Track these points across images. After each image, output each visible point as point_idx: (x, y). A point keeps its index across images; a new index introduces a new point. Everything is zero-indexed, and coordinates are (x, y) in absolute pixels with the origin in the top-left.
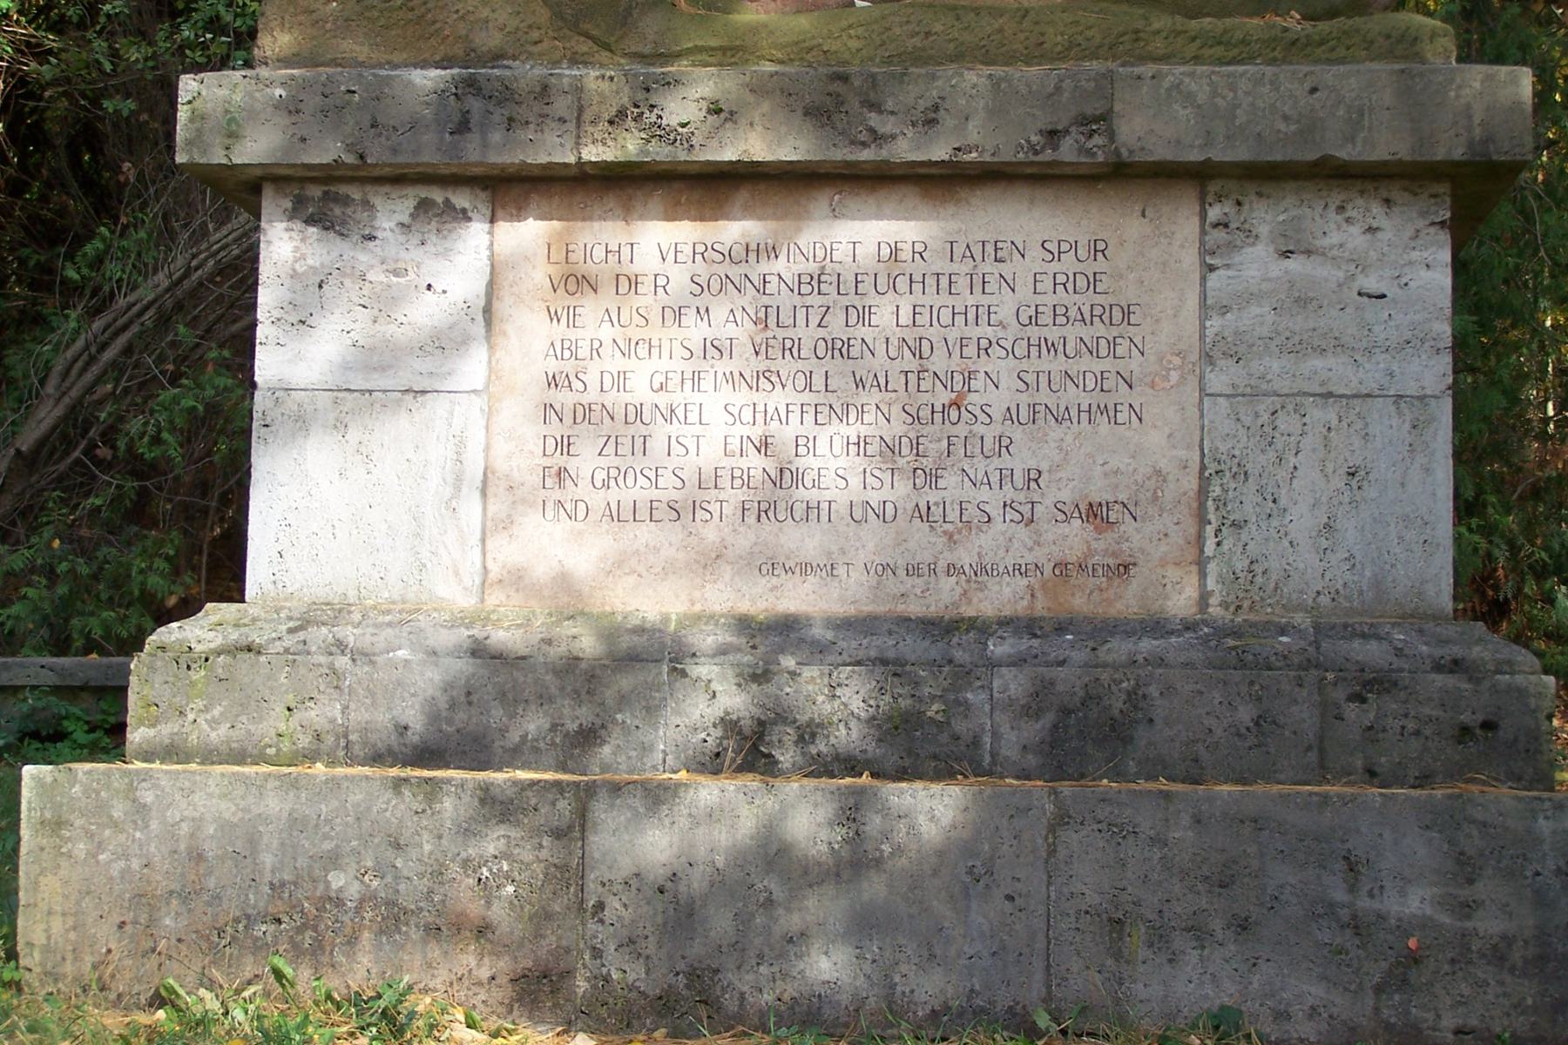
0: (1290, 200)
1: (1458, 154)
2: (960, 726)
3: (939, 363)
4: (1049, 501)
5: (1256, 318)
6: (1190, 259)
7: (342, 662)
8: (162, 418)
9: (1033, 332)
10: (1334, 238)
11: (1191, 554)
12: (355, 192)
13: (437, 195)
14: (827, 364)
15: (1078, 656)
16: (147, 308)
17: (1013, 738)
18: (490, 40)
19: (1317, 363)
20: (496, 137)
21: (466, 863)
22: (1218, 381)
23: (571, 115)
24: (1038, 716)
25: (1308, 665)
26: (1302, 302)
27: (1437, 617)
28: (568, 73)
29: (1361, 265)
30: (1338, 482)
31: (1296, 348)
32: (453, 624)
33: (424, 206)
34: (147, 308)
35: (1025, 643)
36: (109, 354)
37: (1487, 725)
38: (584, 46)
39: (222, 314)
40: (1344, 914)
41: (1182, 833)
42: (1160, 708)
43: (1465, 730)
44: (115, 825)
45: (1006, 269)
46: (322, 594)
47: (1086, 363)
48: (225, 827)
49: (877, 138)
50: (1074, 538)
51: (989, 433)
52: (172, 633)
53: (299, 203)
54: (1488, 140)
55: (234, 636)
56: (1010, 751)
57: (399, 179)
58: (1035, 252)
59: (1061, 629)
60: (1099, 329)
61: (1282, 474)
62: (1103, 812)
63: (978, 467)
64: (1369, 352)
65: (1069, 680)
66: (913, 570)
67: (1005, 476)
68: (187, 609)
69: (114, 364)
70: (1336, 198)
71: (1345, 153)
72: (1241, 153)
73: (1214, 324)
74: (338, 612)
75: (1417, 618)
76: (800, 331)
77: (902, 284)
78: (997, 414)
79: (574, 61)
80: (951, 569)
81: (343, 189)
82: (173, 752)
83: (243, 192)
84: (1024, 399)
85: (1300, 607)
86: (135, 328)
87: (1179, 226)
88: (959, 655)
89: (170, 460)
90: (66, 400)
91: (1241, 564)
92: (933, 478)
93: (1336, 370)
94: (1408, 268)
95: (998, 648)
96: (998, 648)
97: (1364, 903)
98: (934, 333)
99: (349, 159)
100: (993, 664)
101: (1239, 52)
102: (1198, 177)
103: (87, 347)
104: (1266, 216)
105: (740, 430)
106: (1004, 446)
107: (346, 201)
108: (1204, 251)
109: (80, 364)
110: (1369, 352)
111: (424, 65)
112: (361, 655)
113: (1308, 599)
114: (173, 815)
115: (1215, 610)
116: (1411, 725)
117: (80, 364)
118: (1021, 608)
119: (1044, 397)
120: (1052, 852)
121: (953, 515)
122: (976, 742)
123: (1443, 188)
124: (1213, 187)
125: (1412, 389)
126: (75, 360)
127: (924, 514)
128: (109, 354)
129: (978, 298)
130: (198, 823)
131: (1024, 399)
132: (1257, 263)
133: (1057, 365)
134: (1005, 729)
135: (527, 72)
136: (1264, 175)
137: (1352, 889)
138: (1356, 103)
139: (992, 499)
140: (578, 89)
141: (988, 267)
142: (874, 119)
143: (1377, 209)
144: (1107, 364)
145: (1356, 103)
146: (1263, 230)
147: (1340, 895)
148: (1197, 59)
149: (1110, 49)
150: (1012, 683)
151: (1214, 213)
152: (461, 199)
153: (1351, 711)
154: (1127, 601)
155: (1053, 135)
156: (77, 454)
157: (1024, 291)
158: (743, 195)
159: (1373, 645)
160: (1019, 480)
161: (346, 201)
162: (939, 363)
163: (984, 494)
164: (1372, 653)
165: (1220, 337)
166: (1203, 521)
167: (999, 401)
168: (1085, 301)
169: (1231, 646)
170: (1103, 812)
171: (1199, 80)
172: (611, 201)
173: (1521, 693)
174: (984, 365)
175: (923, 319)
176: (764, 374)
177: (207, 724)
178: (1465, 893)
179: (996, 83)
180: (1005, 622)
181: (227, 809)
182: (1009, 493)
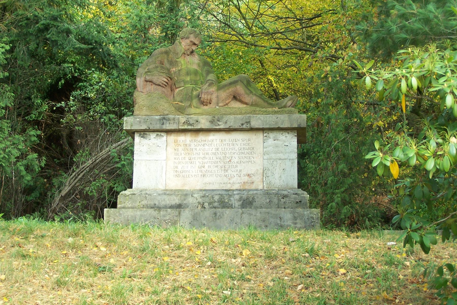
0: (275, 133)
1: (296, 126)
2: (230, 203)
3: (227, 155)
4: (243, 174)
5: (270, 149)
6: (262, 141)
7: (147, 196)
8: (93, 187)
9: (240, 151)
10: (281, 138)
11: (262, 181)
12: (148, 133)
13: (159, 133)
14: (212, 156)
15: (246, 193)
16: (87, 167)
17: (237, 204)
18: (166, 112)
19: (279, 155)
20: (168, 125)
21: (164, 220)
22: (265, 157)
23: (178, 122)
24: (240, 201)
25: (276, 194)
26: (277, 147)
27: (295, 188)
28: (177, 116)
29: (285, 141)
30: (282, 171)
31: (276, 153)
32: (162, 191)
33: (157, 135)
34: (87, 167)
35: (239, 192)
36: (80, 176)
37: (300, 202)
38: (180, 113)
39: (129, 151)
40: (280, 225)
41: (258, 214)
42: (257, 200)
43: (297, 202)
44: (117, 216)
45: (237, 143)
46: (144, 188)
47: (248, 155)
48: (132, 216)
49: (219, 125)
50: (246, 179)
51: (235, 165)
52: (123, 192)
53: (140, 135)
54: (300, 124)
55: (132, 193)
56: (237, 206)
57: (154, 131)
58: (241, 140)
59: (244, 190)
60: (249, 151)
61: (274, 170)
62: (248, 212)
63: (233, 169)
64: (286, 153)
65: (245, 196)
66: (224, 183)
67: (237, 171)
68: (125, 190)
69: (81, 178)
70: (281, 133)
71: (281, 126)
72: (268, 126)
73: (265, 150)
74: (146, 190)
75: (292, 189)
76: (209, 151)
77: (223, 145)
78: (236, 162)
79: (178, 115)
80: (229, 183)
81: (146, 133)
82: (124, 208)
83: (132, 133)
84: (239, 160)
85: (277, 188)
86: (85, 171)
87: (260, 136)
88: (230, 193)
89: (94, 195)
90: (71, 186)
91: (268, 182)
92: (227, 171)
93: (281, 156)
94: (290, 142)
95: (234, 192)
96: (234, 192)
97: (282, 223)
98: (227, 151)
99: (148, 128)
100: (234, 195)
101: (268, 113)
102: (263, 130)
103: (75, 175)
104: (272, 135)
105: (201, 165)
106: (236, 166)
107: (147, 134)
108: (264, 140)
109: (74, 178)
110: (286, 153)
111: (157, 116)
112: (150, 195)
113: (278, 186)
114: (125, 215)
115: (265, 188)
116: (290, 202)
117: (74, 178)
118: (239, 188)
119: (242, 160)
120: (241, 217)
121: (230, 176)
122: (232, 205)
123: (296, 131)
124: (265, 131)
125: (292, 158)
126: (72, 178)
127: (226, 176)
128: (80, 176)
129: (233, 147)
130: (128, 216)
131: (239, 160)
132: (270, 142)
133: (244, 155)
134: (236, 203)
135: (171, 116)
136: (271, 130)
137: (281, 221)
138: (284, 120)
139: (235, 174)
140: (179, 119)
141: (234, 142)
142: (218, 123)
143: (287, 134)
144: (251, 155)
145: (284, 120)
146: (272, 137)
147: (279, 222)
148: (262, 114)
149: (251, 113)
150: (237, 197)
151: (265, 135)
152: (162, 134)
153: (282, 200)
154: (253, 187)
155: (242, 124)
156: (73, 196)
157: (239, 145)
158: (201, 133)
159: (285, 192)
160: (239, 171)
161: (147, 134)
162: (227, 155)
163: (234, 173)
164: (285, 193)
165: (266, 151)
166: (263, 176)
167: (236, 160)
168: (247, 147)
169: (267, 193)
170: (248, 212)
171: (262, 117)
172: (183, 134)
173: (305, 197)
174: (234, 156)
175: (225, 150)
176: (204, 157)
177: (128, 204)
178: (295, 222)
179: (235, 117)
180: (236, 190)
181: (132, 214)
182: (237, 173)
